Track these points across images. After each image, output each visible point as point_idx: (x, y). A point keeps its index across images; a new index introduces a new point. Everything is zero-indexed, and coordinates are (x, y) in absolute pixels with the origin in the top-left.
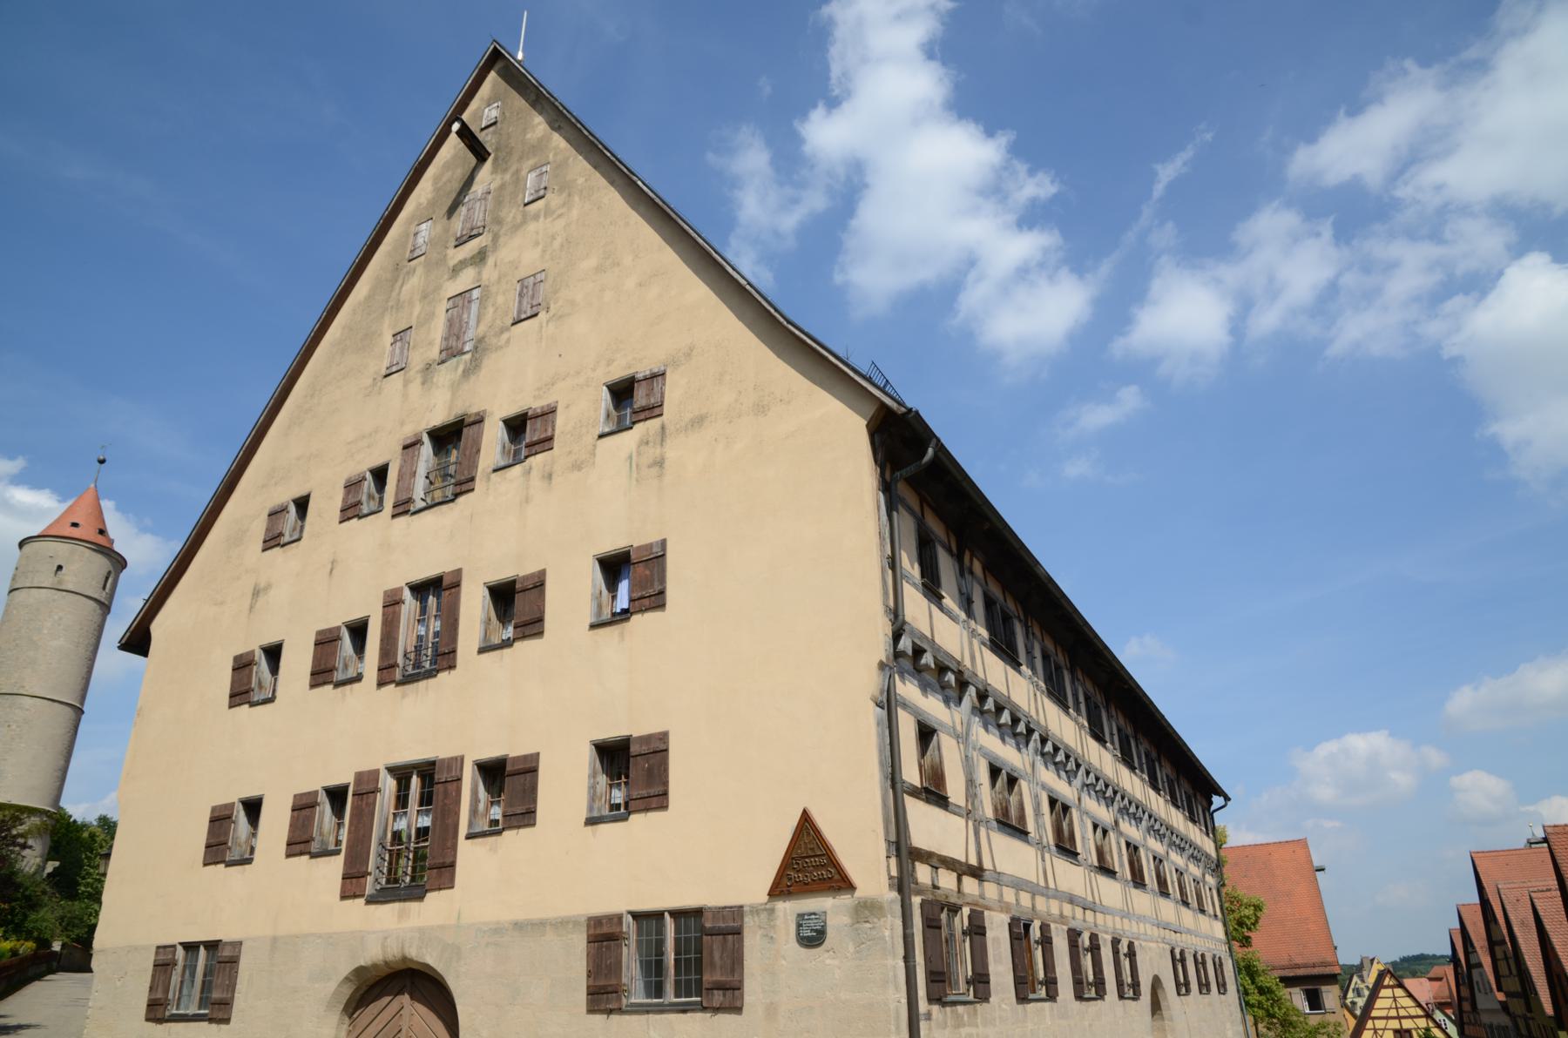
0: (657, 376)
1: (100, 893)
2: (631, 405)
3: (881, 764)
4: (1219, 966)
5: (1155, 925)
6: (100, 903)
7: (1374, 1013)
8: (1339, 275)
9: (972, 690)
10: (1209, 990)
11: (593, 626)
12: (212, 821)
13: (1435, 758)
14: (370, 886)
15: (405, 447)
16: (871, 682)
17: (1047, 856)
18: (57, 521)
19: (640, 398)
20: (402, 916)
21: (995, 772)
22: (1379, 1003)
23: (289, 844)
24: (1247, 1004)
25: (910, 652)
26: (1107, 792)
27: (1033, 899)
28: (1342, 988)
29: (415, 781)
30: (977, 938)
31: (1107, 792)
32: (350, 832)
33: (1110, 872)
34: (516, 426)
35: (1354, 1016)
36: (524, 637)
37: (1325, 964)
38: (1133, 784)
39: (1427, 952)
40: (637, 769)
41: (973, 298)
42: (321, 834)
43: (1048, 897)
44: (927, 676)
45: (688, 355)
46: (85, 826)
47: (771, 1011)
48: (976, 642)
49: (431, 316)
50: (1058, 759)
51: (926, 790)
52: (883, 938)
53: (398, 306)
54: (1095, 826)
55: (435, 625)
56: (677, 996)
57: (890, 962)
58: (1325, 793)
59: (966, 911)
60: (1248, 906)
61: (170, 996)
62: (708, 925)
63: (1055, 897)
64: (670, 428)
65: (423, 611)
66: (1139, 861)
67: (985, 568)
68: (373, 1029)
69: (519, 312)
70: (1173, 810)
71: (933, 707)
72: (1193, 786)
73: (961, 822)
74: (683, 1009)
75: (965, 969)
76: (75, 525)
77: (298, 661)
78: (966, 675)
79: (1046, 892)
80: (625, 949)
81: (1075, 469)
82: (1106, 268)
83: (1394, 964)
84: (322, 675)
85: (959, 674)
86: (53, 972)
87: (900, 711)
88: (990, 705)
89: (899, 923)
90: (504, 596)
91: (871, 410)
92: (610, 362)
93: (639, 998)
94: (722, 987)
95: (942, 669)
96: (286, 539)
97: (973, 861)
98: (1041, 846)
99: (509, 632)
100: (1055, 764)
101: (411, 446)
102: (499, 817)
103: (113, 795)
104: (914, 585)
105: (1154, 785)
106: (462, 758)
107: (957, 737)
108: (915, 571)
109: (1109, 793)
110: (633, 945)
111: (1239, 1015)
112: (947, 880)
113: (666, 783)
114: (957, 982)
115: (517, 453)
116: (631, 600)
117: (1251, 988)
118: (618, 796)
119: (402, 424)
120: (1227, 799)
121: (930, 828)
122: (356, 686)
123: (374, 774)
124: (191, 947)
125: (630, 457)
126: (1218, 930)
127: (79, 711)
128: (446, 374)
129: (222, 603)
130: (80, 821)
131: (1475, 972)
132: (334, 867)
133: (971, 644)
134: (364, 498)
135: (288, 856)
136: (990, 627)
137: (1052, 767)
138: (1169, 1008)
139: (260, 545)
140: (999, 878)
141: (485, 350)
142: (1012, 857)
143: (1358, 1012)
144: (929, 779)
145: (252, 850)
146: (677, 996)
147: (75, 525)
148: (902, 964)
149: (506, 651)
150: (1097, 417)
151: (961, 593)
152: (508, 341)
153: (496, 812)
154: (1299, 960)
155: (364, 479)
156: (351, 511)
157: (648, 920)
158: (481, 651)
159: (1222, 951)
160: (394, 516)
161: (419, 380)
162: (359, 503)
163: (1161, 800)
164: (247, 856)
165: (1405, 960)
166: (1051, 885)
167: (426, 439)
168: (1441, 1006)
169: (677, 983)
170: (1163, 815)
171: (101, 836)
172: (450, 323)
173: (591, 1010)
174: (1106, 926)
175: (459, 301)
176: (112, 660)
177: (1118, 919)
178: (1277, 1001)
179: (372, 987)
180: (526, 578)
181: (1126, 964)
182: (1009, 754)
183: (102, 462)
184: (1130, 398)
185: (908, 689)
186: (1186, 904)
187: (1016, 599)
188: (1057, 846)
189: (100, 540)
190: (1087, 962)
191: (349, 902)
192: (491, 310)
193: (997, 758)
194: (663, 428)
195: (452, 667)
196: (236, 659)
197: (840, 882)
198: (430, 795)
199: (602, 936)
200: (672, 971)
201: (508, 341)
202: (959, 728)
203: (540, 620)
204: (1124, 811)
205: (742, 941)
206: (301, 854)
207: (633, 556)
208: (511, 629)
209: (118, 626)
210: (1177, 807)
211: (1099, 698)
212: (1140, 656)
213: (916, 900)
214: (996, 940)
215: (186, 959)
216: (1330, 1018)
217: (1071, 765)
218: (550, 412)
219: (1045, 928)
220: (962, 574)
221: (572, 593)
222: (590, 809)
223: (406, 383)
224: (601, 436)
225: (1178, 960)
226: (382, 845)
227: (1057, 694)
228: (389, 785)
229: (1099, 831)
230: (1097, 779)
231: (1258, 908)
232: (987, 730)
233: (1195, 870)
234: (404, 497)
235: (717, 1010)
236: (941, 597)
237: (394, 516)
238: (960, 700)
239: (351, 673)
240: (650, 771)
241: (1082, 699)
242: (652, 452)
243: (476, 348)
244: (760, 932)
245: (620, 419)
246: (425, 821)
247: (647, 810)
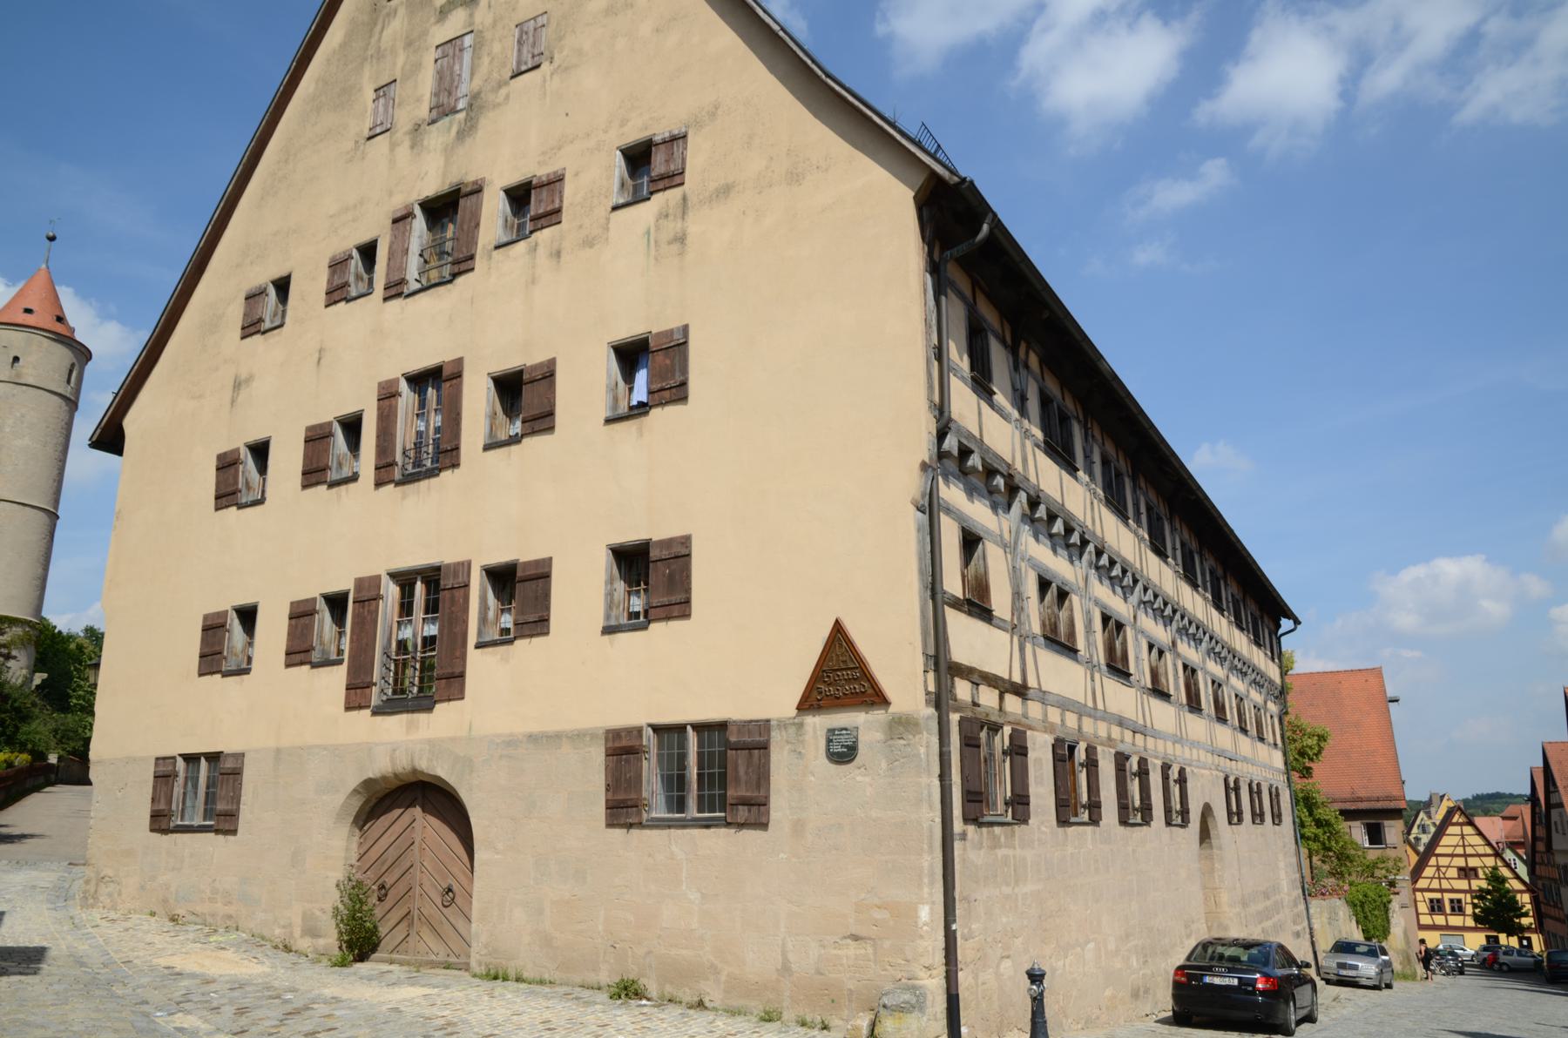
0: (678, 139)
1: (92, 705)
2: (648, 174)
3: (921, 572)
4: (1275, 796)
5: (1210, 752)
6: (92, 714)
7: (1439, 850)
8: (1484, 20)
9: (1022, 496)
10: (1262, 821)
11: (608, 421)
12: (205, 629)
13: (1536, 586)
14: (375, 697)
15: (395, 221)
16: (911, 483)
17: (1097, 676)
18: (8, 306)
19: (659, 164)
20: (410, 727)
21: (1044, 585)
22: (1445, 841)
23: (288, 654)
24: (1302, 836)
25: (955, 452)
26: (1166, 611)
27: (1080, 719)
28: (1406, 823)
29: (419, 587)
30: (1018, 758)
31: (1166, 611)
32: (352, 641)
33: (1164, 695)
34: (519, 196)
35: (1417, 852)
36: (533, 433)
37: (1389, 799)
38: (1195, 603)
39: (1503, 790)
40: (657, 574)
41: (1035, 53)
42: (322, 643)
43: (1096, 719)
44: (973, 479)
45: (713, 115)
46: (70, 637)
47: (798, 827)
48: (1028, 444)
49: (417, 67)
50: (1114, 573)
51: (969, 602)
52: (918, 755)
53: (380, 55)
54: (1151, 647)
55: (436, 420)
56: (700, 811)
57: (924, 780)
58: (1406, 621)
59: (1007, 730)
60: (1311, 736)
61: (174, 807)
62: (733, 739)
63: (1104, 719)
64: (692, 200)
65: (422, 404)
66: (1196, 684)
67: (1041, 362)
68: (384, 842)
69: (519, 63)
70: (1237, 632)
71: (980, 513)
72: (1261, 607)
73: (1005, 636)
74: (707, 824)
75: (1003, 789)
76: (28, 311)
77: (287, 460)
78: (1017, 480)
79: (1094, 713)
80: (645, 763)
81: (1147, 255)
82: (1195, 16)
83: (1465, 801)
84: (314, 474)
85: (1009, 478)
86: (52, 784)
87: (942, 516)
88: (1041, 512)
89: (935, 740)
90: (510, 387)
91: (920, 179)
92: (623, 123)
93: (659, 812)
94: (747, 803)
95: (990, 472)
96: (267, 325)
97: (1017, 678)
98: (1091, 665)
99: (517, 427)
100: (1111, 578)
101: (401, 220)
102: (510, 625)
103: (98, 606)
104: (962, 379)
105: (1218, 606)
106: (469, 563)
107: (1005, 546)
108: (964, 364)
109: (1168, 611)
110: (654, 759)
111: (1293, 846)
112: (988, 697)
113: (688, 590)
114: (995, 804)
115: (521, 227)
116: (650, 392)
117: (1308, 820)
118: (637, 604)
119: (391, 194)
120: (1297, 622)
121: (971, 641)
122: (352, 486)
123: (376, 580)
124: (192, 759)
125: (648, 233)
126: (1277, 759)
127: (54, 516)
128: (438, 137)
129: (201, 396)
130: (65, 632)
131: (1554, 813)
132: (337, 677)
133: (1023, 446)
134: (352, 279)
135: (288, 665)
136: (1046, 427)
137: (1106, 582)
138: (1218, 837)
139: (238, 333)
140: (1044, 697)
141: (481, 107)
142: (1058, 676)
143: (1421, 849)
144: (972, 590)
145: (250, 660)
146: (700, 811)
147: (28, 311)
148: (937, 783)
149: (514, 448)
150: (1174, 195)
151: (1014, 389)
152: (507, 97)
153: (507, 621)
154: (1362, 794)
155: (351, 257)
156: (337, 294)
157: (670, 733)
158: (487, 448)
159: (1280, 781)
160: (386, 299)
161: (407, 143)
162: (346, 284)
163: (1224, 621)
164: (244, 666)
165: (1477, 798)
166: (1100, 706)
167: (418, 211)
168: (1513, 846)
169: (701, 798)
170: (1225, 637)
171: (89, 648)
172: (440, 76)
173: (610, 825)
174: (1156, 751)
175: (449, 49)
176: (85, 461)
177: (1169, 744)
178: (1334, 835)
179: (381, 800)
180: (534, 368)
181: (1175, 790)
182: (1061, 567)
183: (52, 239)
184: (1216, 172)
185: (952, 493)
186: (1244, 731)
187: (1077, 398)
188: (1108, 666)
189: (59, 328)
190: (1134, 787)
191: (355, 713)
192: (486, 60)
193: (1048, 570)
194: (684, 199)
195: (455, 465)
196: (220, 457)
197: (874, 697)
198: (436, 601)
199: (622, 749)
200: (695, 786)
201: (507, 97)
202: (1006, 536)
203: (551, 414)
204: (1183, 631)
205: (768, 756)
206: (302, 663)
207: (652, 343)
208: (518, 424)
209: (86, 425)
210: (1242, 629)
211: (1162, 510)
212: (1210, 464)
213: (955, 718)
214: (1038, 761)
215: (187, 770)
216: (1391, 853)
217: (1128, 580)
218: (556, 181)
219: (1090, 750)
220: (1016, 368)
221: (585, 385)
222: (608, 617)
223: (393, 146)
224: (615, 208)
225: (1232, 788)
226: (386, 654)
227: (1116, 503)
228: (392, 591)
229: (1155, 651)
230: (1156, 596)
231: (1322, 738)
232: (1037, 540)
233: (1256, 696)
234: (396, 277)
235: (741, 826)
236: (992, 393)
237: (386, 299)
238: (1009, 506)
239: (346, 472)
240: (671, 577)
241: (1143, 509)
242: (672, 227)
243: (471, 105)
244: (788, 747)
245: (636, 189)
246: (432, 630)
247: (668, 618)
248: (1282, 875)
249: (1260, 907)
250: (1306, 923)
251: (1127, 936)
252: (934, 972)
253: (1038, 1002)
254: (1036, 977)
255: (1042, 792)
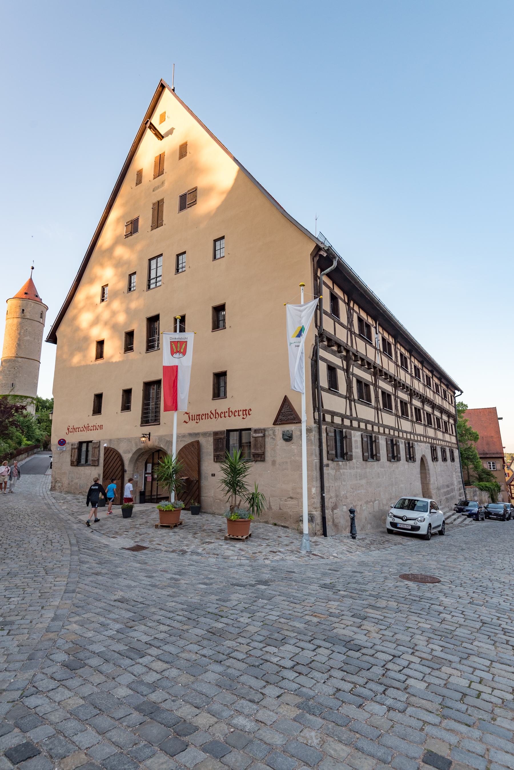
4: (452, 452)
46: (47, 401)
47: (274, 463)
120: (462, 392)
121: (332, 403)
126: (454, 440)
225: (433, 450)
248: (455, 479)
249: (445, 490)
250: (464, 496)
251: (391, 499)
252: (318, 510)
253: (353, 519)
254: (352, 512)
255: (357, 450)
